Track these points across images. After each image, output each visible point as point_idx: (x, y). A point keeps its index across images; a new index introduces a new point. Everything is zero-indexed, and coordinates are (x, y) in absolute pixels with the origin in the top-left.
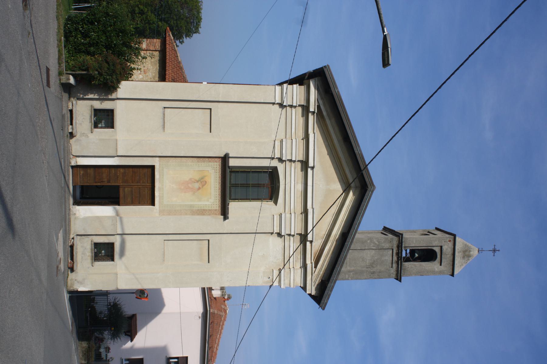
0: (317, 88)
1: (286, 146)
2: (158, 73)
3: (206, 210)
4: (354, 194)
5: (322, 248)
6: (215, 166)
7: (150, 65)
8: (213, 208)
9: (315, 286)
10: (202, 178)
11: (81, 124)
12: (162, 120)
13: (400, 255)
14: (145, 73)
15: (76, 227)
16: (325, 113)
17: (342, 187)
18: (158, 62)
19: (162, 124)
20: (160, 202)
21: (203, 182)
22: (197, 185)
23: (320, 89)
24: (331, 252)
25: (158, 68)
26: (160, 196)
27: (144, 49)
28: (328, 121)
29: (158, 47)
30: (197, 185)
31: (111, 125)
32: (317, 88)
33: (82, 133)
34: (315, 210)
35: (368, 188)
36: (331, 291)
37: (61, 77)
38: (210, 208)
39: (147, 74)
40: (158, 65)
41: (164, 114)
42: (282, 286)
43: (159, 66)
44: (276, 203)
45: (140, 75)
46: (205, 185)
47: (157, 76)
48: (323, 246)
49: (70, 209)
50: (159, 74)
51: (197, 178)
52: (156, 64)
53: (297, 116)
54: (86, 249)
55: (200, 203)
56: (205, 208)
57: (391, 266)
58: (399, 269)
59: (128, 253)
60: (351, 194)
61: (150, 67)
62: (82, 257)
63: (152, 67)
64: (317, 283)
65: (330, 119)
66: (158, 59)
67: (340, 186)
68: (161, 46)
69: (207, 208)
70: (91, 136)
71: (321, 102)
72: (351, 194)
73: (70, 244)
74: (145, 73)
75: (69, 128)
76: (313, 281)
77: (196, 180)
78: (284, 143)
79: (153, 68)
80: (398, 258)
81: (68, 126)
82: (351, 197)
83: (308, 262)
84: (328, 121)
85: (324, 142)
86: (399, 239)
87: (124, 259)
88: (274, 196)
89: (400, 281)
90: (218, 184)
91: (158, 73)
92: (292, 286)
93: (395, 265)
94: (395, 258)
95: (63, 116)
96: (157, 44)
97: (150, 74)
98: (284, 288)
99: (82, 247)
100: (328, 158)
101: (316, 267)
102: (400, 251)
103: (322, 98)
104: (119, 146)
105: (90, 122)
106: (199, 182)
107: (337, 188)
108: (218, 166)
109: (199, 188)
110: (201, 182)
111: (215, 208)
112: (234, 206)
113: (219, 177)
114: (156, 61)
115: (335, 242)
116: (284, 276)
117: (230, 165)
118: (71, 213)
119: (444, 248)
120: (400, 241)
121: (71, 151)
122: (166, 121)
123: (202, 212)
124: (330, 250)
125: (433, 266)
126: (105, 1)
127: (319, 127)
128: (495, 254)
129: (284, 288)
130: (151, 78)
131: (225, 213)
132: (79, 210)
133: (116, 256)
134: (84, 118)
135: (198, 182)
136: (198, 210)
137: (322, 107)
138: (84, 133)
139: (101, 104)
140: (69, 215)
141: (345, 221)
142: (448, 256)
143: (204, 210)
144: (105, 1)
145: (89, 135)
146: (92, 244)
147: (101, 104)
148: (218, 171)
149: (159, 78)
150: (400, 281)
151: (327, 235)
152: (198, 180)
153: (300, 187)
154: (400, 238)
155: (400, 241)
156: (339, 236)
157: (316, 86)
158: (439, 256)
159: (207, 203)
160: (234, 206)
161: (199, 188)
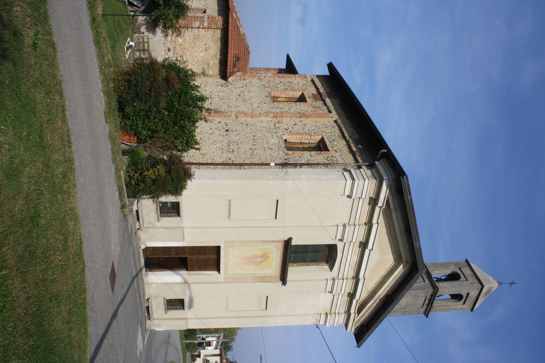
0: (389, 188)
1: (348, 232)
2: (219, 51)
3: (267, 277)
4: (403, 267)
5: (366, 300)
6: (278, 245)
7: (211, 43)
8: (273, 275)
9: (355, 327)
10: (265, 254)
11: (147, 215)
12: (228, 211)
13: (431, 301)
14: (207, 51)
15: (149, 292)
16: (392, 207)
17: (393, 258)
18: (220, 40)
19: (228, 213)
20: (224, 272)
21: (265, 257)
22: (259, 260)
23: (392, 187)
24: (373, 307)
25: (220, 46)
26: (225, 268)
27: (206, 27)
28: (394, 214)
29: (220, 26)
30: (259, 260)
31: (178, 214)
32: (389, 187)
33: (149, 222)
34: (365, 281)
35: (418, 271)
36: (368, 337)
37: (124, 210)
38: (271, 275)
39: (209, 52)
40: (219, 43)
41: (230, 205)
42: (327, 325)
43: (221, 44)
44: (331, 268)
45: (201, 53)
46: (267, 259)
47: (219, 53)
48: (367, 299)
49: (143, 280)
50: (221, 52)
51: (260, 254)
52: (218, 42)
53: (363, 206)
54: (159, 303)
55: (262, 272)
56: (266, 275)
57: (422, 306)
58: (428, 310)
59: (195, 305)
60: (401, 267)
61: (212, 44)
62: (157, 309)
63: (213, 45)
64: (357, 325)
65: (396, 212)
66: (220, 37)
67: (392, 257)
68: (223, 25)
69: (268, 275)
70: (158, 224)
71: (390, 198)
72: (401, 267)
73: (146, 306)
74: (207, 51)
75: (136, 225)
76: (355, 321)
77: (259, 256)
78: (347, 229)
79: (215, 46)
80: (429, 303)
81: (136, 223)
82: (400, 270)
83: (352, 311)
84: (394, 214)
85: (385, 224)
86: (435, 291)
87: (192, 310)
88: (330, 262)
89: (427, 317)
90: (279, 258)
91: (219, 51)
92: (335, 325)
93: (425, 307)
94: (427, 302)
95: (131, 244)
96: (219, 22)
97: (212, 51)
98: (329, 326)
99: (156, 302)
100: (386, 236)
101: (358, 314)
102: (432, 299)
103: (392, 195)
104: (185, 234)
105: (156, 213)
106: (262, 257)
107: (389, 260)
108: (281, 245)
109: (262, 262)
110: (264, 257)
111: (275, 275)
112: (294, 271)
113: (281, 253)
114: (218, 39)
115: (378, 300)
116: (330, 320)
117: (292, 244)
118: (144, 282)
119: (470, 294)
120: (435, 292)
121: (140, 238)
122: (231, 210)
123: (263, 279)
124: (372, 304)
125: (459, 305)
126: (161, 2)
127: (382, 217)
128: (512, 286)
129: (329, 326)
130: (212, 56)
131: (283, 279)
132: (151, 279)
133: (186, 308)
134: (150, 210)
135: (260, 257)
136: (260, 277)
137: (391, 202)
138: (151, 222)
139: (166, 198)
140: (143, 283)
141: (391, 287)
142: (472, 299)
143: (265, 276)
144: (161, 2)
145: (156, 224)
146: (164, 301)
147: (166, 198)
148: (280, 249)
149: (220, 55)
150: (427, 317)
151: (372, 291)
152: (261, 255)
153: (355, 259)
154: (436, 291)
155: (435, 292)
156: (383, 296)
157: (389, 186)
158: (464, 299)
159: (268, 272)
160: (294, 271)
161: (262, 262)
